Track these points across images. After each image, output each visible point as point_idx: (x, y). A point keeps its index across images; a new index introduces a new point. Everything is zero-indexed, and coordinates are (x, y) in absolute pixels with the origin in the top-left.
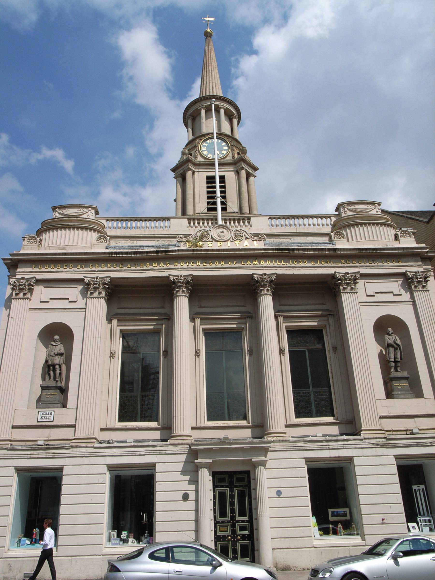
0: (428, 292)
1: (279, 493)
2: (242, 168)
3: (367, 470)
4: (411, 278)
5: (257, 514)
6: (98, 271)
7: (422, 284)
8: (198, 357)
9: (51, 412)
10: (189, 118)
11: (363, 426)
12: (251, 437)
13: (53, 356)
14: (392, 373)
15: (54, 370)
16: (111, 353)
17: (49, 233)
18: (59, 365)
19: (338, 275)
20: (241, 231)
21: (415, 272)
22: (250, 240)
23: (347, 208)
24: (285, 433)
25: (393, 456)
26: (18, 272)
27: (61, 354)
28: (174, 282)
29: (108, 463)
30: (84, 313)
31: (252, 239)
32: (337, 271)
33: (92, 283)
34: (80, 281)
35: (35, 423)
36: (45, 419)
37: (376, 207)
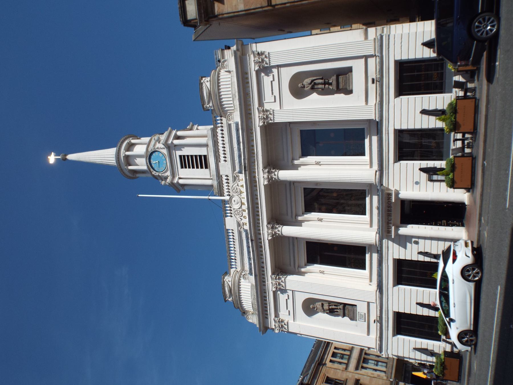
0: (270, 53)
1: (417, 183)
2: (172, 143)
3: (404, 120)
7: (264, 58)
8: (322, 219)
14: (333, 88)
16: (319, 220)
17: (242, 300)
19: (256, 69)
20: (233, 188)
21: (255, 63)
23: (207, 105)
26: (271, 327)
27: (323, 305)
28: (272, 236)
30: (295, 292)
31: (238, 181)
32: (253, 70)
33: (276, 286)
34: (275, 293)
35: (366, 323)
37: (204, 82)
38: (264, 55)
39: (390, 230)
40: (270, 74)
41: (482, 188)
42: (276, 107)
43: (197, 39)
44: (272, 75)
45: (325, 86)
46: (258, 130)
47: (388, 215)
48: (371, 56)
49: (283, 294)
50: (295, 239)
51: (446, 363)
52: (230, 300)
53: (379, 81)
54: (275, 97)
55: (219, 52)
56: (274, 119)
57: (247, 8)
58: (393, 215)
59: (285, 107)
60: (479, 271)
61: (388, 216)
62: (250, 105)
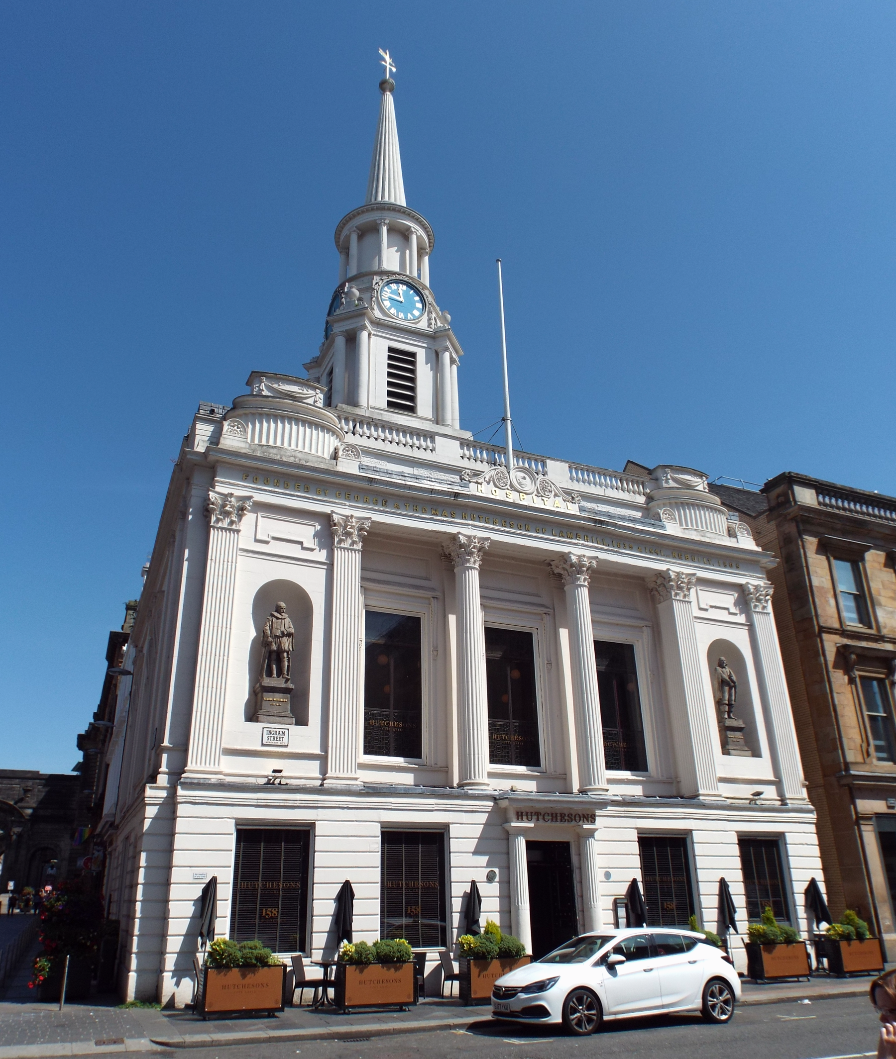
0: (238, 534)
3: (361, 844)
9: (283, 730)
10: (354, 231)
12: (642, 794)
13: (278, 637)
18: (288, 653)
19: (335, 516)
21: (347, 517)
22: (561, 499)
24: (607, 790)
25: (734, 833)
26: (218, 482)
29: (639, 826)
32: (336, 510)
36: (274, 741)
38: (236, 520)
39: (525, 818)
40: (737, 608)
41: (755, 1003)
42: (245, 540)
44: (737, 612)
46: (453, 530)
47: (554, 815)
48: (324, 771)
49: (314, 536)
50: (432, 593)
51: (264, 971)
52: (263, 386)
53: (322, 785)
54: (267, 542)
56: (341, 548)
57: (815, 589)
58: (554, 824)
59: (243, 562)
60: (595, 1018)
61: (552, 814)
62: (693, 561)
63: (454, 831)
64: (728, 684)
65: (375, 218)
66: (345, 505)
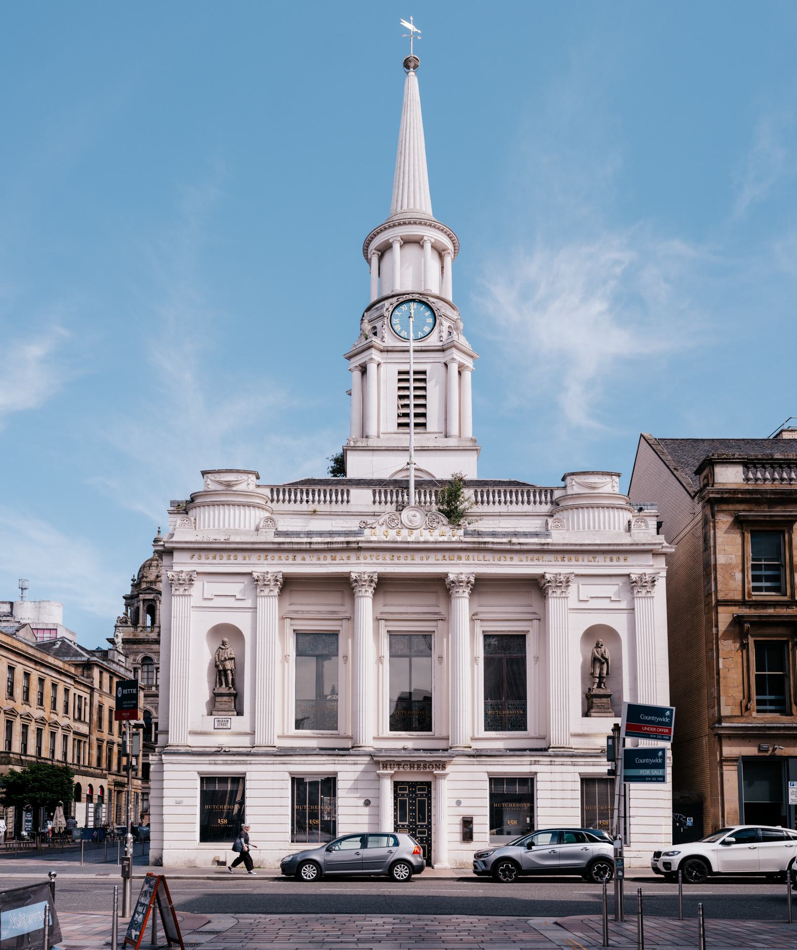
1: (459, 803)
4: (635, 582)
5: (435, 820)
6: (267, 564)
10: (374, 254)
11: (552, 743)
15: (226, 676)
18: (231, 670)
43: (642, 438)
45: (598, 678)
55: (654, 511)
63: (340, 777)
64: (599, 660)
65: (388, 238)
66: (264, 564)
